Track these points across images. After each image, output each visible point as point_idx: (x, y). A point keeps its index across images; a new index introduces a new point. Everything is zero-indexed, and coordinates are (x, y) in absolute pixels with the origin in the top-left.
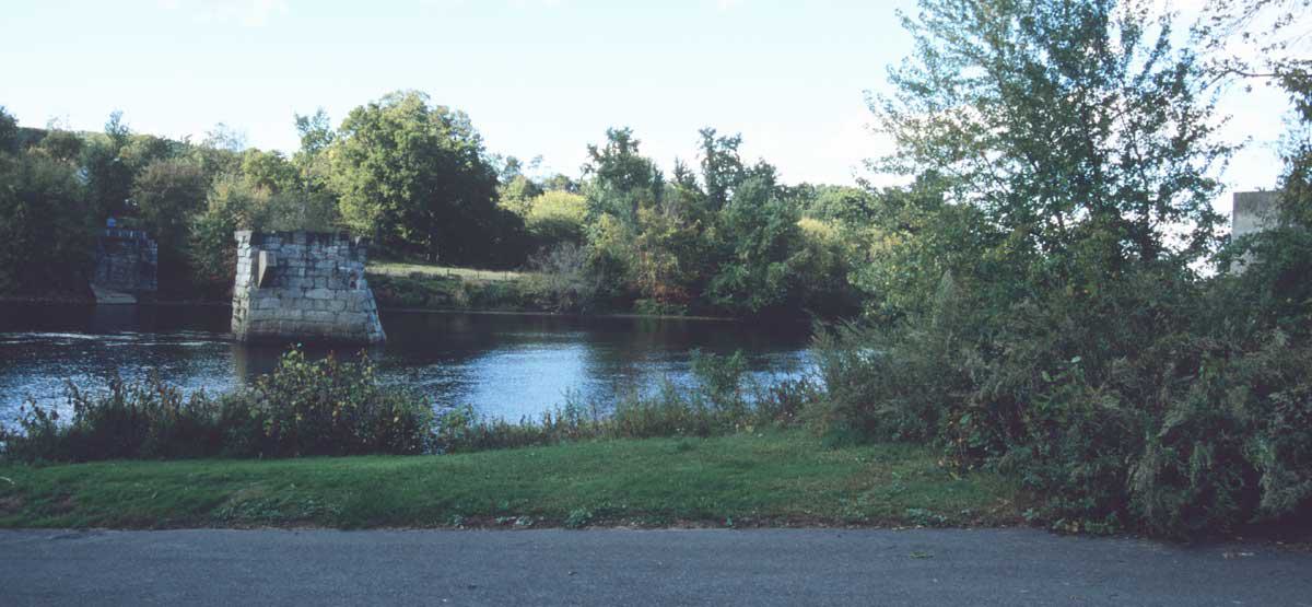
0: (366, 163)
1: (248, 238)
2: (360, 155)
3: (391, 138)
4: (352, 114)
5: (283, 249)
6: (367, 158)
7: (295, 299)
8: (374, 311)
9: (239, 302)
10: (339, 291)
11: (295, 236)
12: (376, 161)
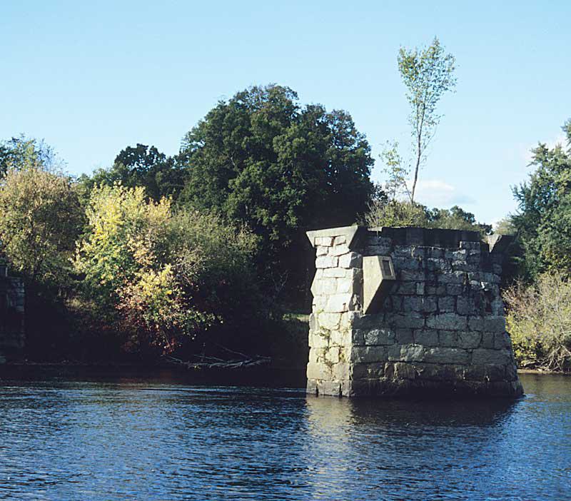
3: (268, 146)
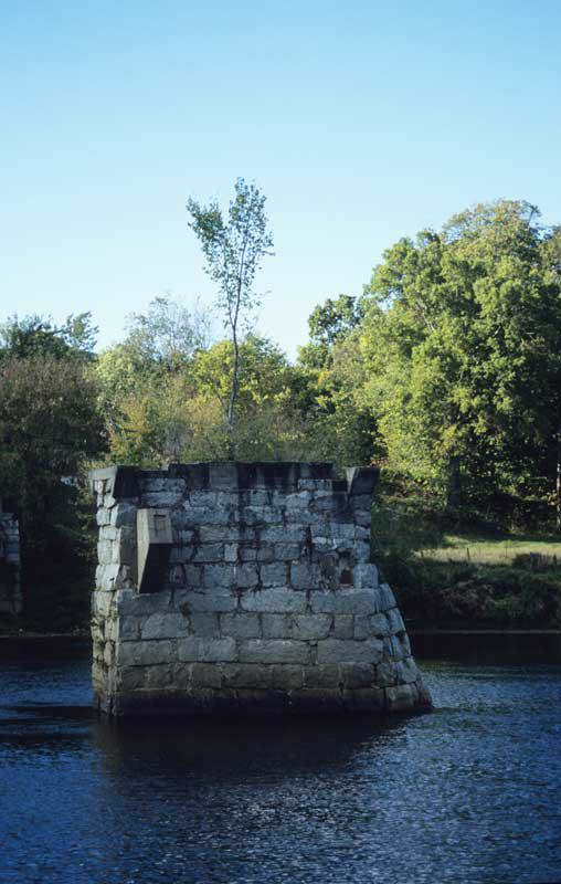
0: (423, 347)
1: (111, 484)
2: (412, 332)
4: (388, 255)
5: (187, 505)
6: (423, 338)
7: (219, 614)
8: (400, 635)
9: (102, 627)
10: (315, 594)
11: (212, 473)
12: (442, 343)
